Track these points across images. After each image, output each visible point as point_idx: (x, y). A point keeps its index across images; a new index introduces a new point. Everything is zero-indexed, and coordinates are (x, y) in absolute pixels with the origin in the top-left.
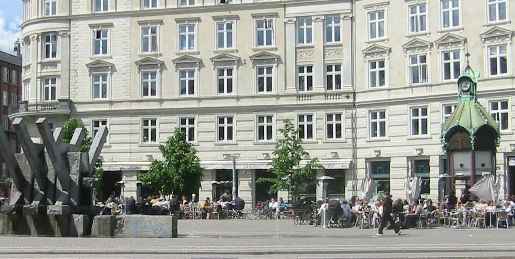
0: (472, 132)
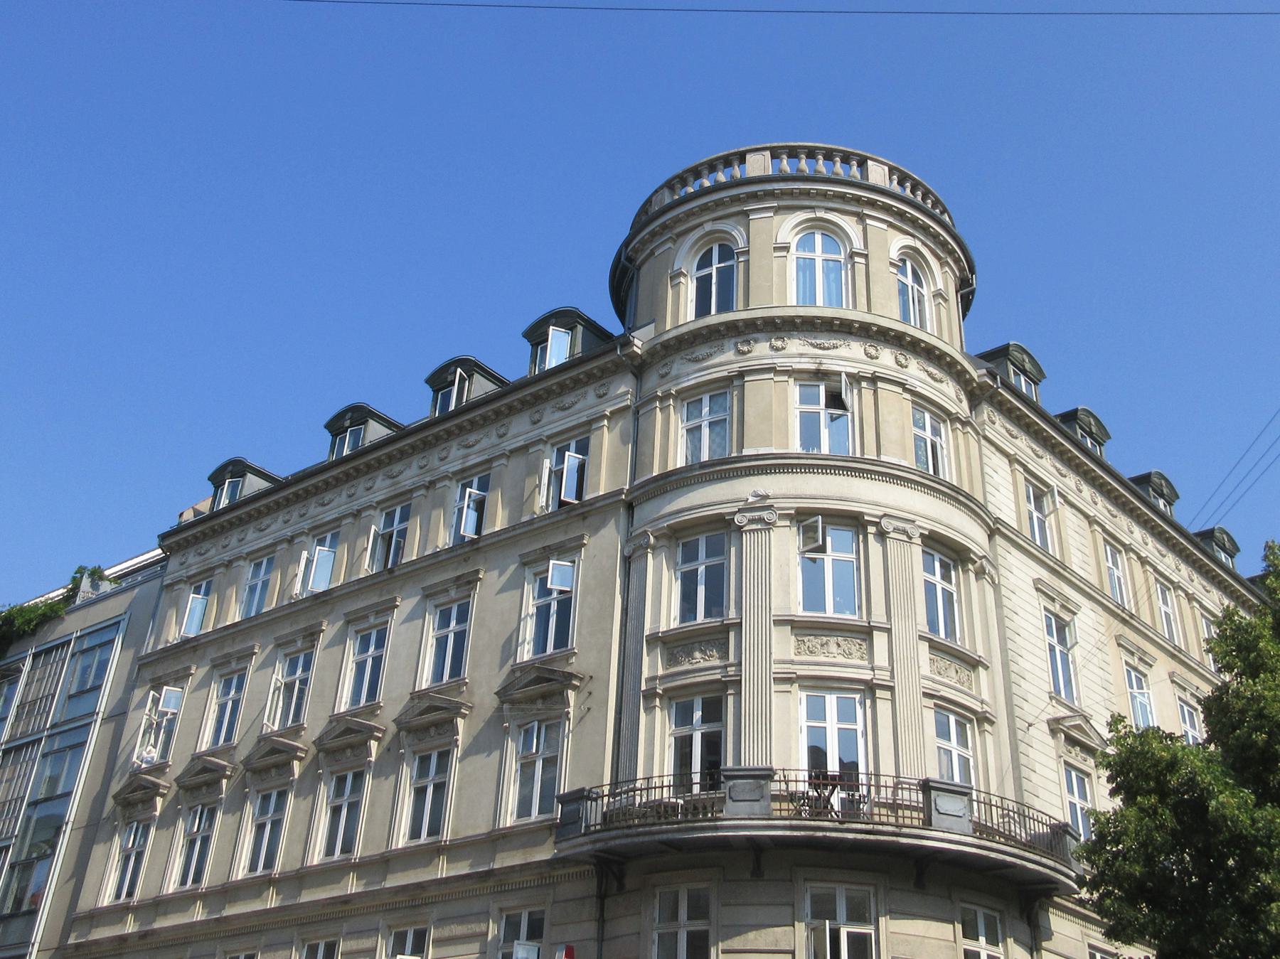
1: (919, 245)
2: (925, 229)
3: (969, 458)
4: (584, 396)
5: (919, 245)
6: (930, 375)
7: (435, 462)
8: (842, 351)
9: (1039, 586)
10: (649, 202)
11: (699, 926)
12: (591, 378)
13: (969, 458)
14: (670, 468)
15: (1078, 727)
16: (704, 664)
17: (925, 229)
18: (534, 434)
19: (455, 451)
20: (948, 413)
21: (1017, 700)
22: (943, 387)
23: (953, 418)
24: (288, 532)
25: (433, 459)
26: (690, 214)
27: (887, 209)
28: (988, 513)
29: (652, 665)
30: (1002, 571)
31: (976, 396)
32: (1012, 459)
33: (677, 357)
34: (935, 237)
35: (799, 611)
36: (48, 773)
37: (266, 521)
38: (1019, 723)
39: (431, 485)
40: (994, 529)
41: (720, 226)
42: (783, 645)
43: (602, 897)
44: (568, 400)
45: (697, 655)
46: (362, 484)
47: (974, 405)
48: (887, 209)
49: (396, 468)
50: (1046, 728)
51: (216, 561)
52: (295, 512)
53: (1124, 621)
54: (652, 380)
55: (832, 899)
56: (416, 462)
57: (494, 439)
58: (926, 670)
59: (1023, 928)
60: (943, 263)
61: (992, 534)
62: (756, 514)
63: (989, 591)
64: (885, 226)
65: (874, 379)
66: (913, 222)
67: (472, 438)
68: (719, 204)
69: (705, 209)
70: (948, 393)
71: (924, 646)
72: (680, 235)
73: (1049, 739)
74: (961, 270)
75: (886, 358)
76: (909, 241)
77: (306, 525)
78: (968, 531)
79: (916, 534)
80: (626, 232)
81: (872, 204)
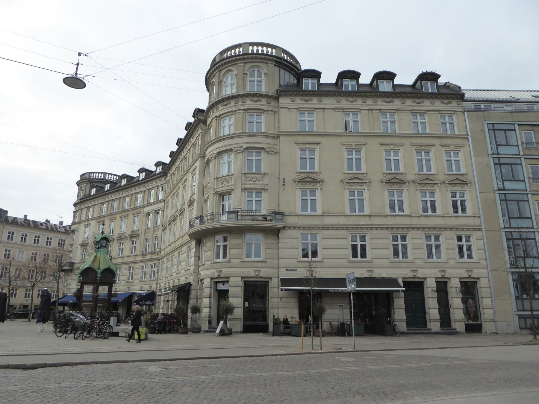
0: (99, 272)
10: (215, 58)
11: (225, 243)
80: (209, 68)
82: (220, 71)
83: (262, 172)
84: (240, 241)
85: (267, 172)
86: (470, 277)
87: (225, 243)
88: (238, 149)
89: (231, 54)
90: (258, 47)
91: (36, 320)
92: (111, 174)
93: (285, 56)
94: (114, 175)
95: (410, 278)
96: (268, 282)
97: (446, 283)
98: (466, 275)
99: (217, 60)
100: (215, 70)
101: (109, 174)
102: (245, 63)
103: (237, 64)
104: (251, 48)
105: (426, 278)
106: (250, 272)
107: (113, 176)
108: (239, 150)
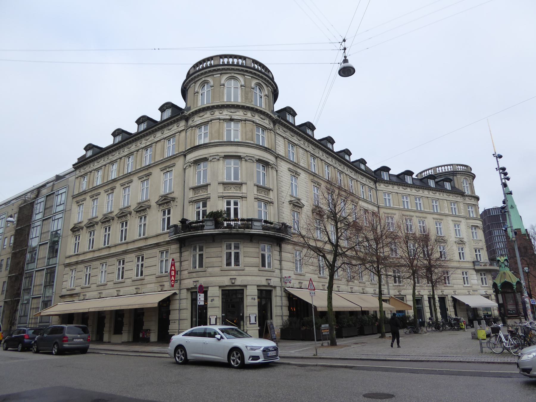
1: (260, 82)
2: (262, 77)
3: (271, 139)
4: (174, 126)
5: (260, 82)
6: (261, 118)
7: (139, 144)
8: (237, 113)
9: (290, 170)
10: (189, 71)
11: (201, 253)
12: (175, 122)
13: (271, 139)
14: (95, 185)
15: (297, 202)
16: (202, 194)
17: (262, 77)
18: (162, 137)
19: (144, 141)
20: (266, 128)
21: (280, 197)
22: (265, 121)
23: (267, 129)
24: (104, 163)
25: (138, 143)
26: (198, 76)
27: (251, 72)
28: (275, 153)
29: (191, 195)
30: (279, 167)
31: (275, 122)
32: (284, 138)
33: (196, 116)
34: (265, 79)
35: (225, 181)
36: (479, 225)
37: (99, 160)
38: (280, 203)
39: (138, 151)
40: (277, 156)
41: (206, 79)
42: (221, 189)
43: (181, 248)
44: (170, 127)
45: (201, 192)
46: (121, 150)
47: (274, 125)
48: (251, 72)
49: (130, 146)
50: (288, 203)
51: (88, 171)
52: (106, 158)
53: (314, 176)
54: (190, 123)
55: (231, 245)
56: (134, 144)
57: (153, 138)
58: (256, 193)
59: (278, 248)
60: (267, 86)
61: (276, 158)
62: (214, 157)
63: (275, 172)
64: (219, 75)
65: (245, 120)
66: (259, 76)
67: (147, 138)
68: (206, 73)
69: (202, 74)
70: (266, 123)
71: (256, 188)
72: (196, 81)
73: (289, 206)
74: (273, 87)
75: (249, 115)
76: (258, 81)
77: (109, 161)
78: (270, 158)
79: (254, 160)
80: (185, 78)
81: (247, 71)
82: (195, 83)
83: (239, 181)
84: (219, 249)
85: (244, 181)
86: (269, 285)
87: (201, 253)
88: (214, 157)
89: (207, 65)
90: (228, 59)
91: (125, 337)
92: (444, 166)
93: (256, 65)
94: (447, 165)
95: (227, 286)
96: (243, 290)
97: (270, 292)
98: (264, 283)
99: (191, 73)
100: (190, 81)
101: (438, 167)
102: (221, 74)
103: (213, 75)
104: (221, 60)
105: (246, 286)
106: (226, 281)
107: (449, 167)
108: (215, 158)
